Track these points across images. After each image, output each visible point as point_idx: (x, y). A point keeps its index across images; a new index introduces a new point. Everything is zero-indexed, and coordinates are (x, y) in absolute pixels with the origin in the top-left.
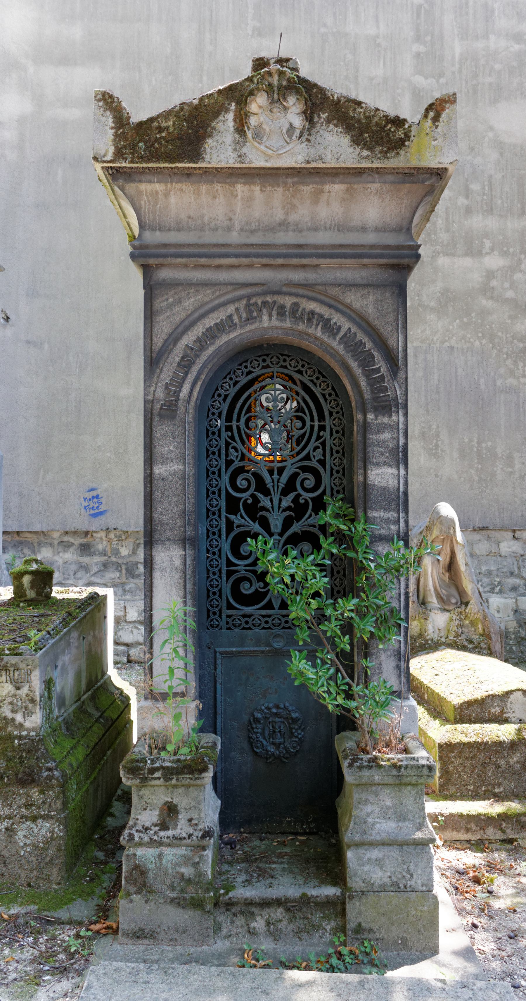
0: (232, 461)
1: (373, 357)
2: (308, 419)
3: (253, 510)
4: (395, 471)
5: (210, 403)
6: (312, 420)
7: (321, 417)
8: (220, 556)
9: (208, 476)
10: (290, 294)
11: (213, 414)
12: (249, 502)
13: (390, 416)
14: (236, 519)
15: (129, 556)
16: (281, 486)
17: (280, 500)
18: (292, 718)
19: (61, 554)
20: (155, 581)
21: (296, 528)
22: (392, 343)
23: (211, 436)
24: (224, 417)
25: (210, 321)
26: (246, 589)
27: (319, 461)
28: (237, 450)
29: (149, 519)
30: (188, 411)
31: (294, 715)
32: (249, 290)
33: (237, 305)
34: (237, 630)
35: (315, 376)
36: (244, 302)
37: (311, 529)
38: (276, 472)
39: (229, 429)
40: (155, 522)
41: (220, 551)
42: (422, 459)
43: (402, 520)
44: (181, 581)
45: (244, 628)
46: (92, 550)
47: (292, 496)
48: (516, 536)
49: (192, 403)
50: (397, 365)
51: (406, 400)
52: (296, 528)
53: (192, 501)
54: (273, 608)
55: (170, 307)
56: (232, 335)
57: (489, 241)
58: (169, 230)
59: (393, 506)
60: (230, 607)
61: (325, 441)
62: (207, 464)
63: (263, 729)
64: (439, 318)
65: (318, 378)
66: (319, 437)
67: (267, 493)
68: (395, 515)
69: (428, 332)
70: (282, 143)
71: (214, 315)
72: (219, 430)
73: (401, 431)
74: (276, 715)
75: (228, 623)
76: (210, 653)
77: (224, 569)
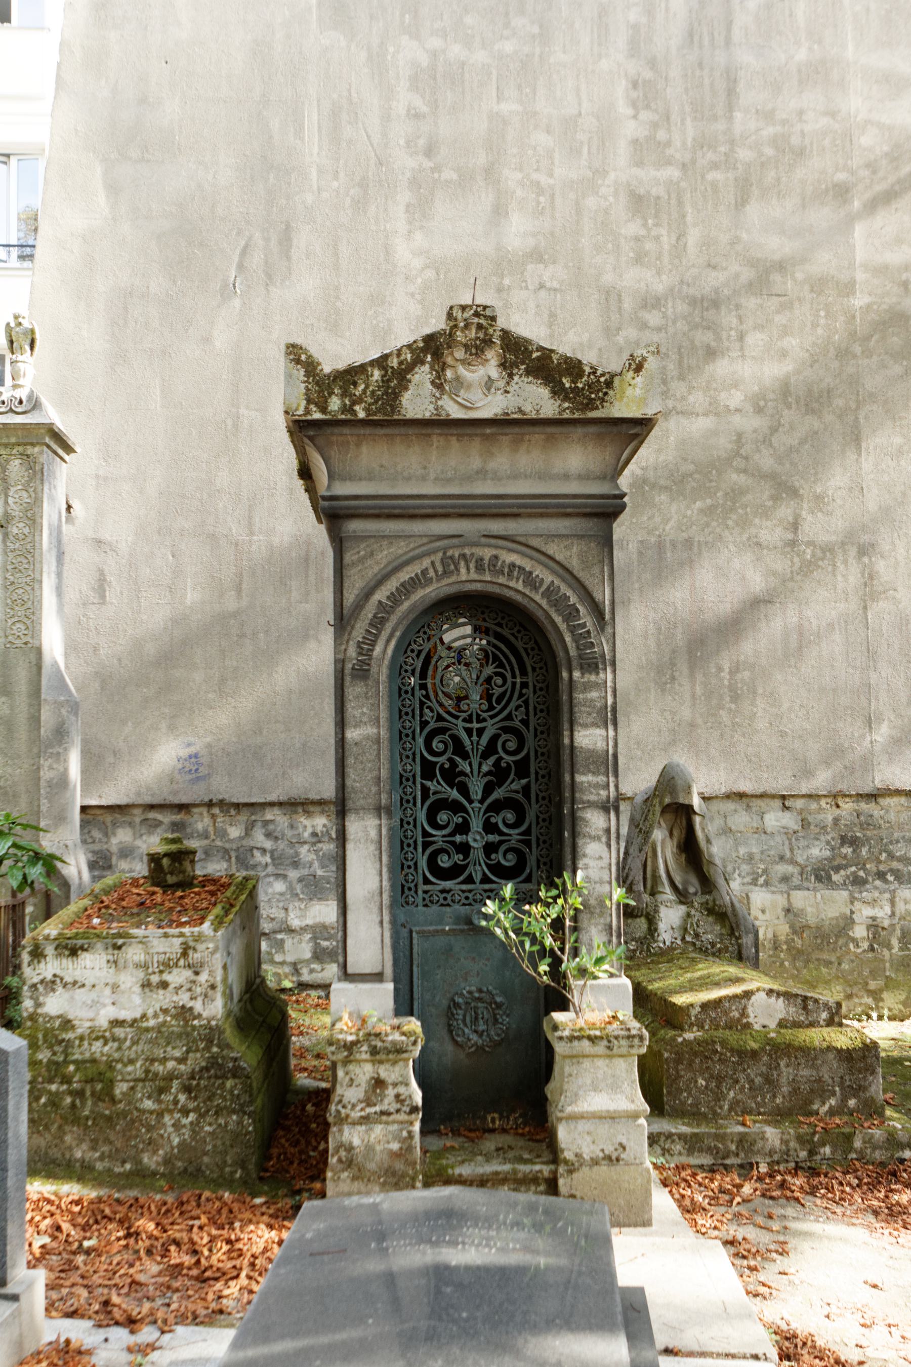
0: (427, 723)
1: (578, 611)
2: (509, 676)
3: (451, 776)
4: (603, 732)
5: (402, 659)
6: (514, 676)
7: (524, 673)
8: (415, 826)
9: (401, 739)
10: (489, 546)
11: (406, 671)
12: (447, 766)
13: (598, 674)
14: (432, 785)
15: (241, 838)
16: (481, 748)
17: (480, 765)
18: (496, 1003)
19: (144, 837)
20: (348, 853)
21: (499, 794)
22: (598, 596)
23: (404, 695)
24: (417, 674)
25: (405, 575)
26: (444, 862)
27: (522, 721)
28: (432, 711)
29: (342, 786)
30: (382, 671)
31: (498, 999)
32: (446, 542)
33: (433, 558)
34: (435, 908)
35: (516, 630)
36: (440, 554)
37: (514, 795)
38: (475, 733)
39: (423, 687)
40: (348, 790)
41: (415, 820)
42: (652, 697)
43: (612, 785)
44: (377, 852)
45: (442, 905)
46: (189, 830)
47: (491, 760)
48: (787, 803)
49: (386, 662)
50: (604, 619)
51: (614, 656)
52: (499, 794)
53: (387, 766)
54: (473, 882)
55: (362, 560)
56: (428, 590)
57: (739, 393)
58: (360, 479)
59: (603, 770)
60: (426, 881)
61: (527, 699)
62: (400, 725)
63: (464, 1016)
64: (673, 499)
65: (519, 632)
66: (521, 695)
67: (465, 756)
68: (605, 779)
69: (657, 519)
70: (483, 396)
71: (409, 568)
72: (413, 689)
73: (609, 690)
74: (480, 999)
75: (424, 899)
76: (404, 932)
77: (420, 840)
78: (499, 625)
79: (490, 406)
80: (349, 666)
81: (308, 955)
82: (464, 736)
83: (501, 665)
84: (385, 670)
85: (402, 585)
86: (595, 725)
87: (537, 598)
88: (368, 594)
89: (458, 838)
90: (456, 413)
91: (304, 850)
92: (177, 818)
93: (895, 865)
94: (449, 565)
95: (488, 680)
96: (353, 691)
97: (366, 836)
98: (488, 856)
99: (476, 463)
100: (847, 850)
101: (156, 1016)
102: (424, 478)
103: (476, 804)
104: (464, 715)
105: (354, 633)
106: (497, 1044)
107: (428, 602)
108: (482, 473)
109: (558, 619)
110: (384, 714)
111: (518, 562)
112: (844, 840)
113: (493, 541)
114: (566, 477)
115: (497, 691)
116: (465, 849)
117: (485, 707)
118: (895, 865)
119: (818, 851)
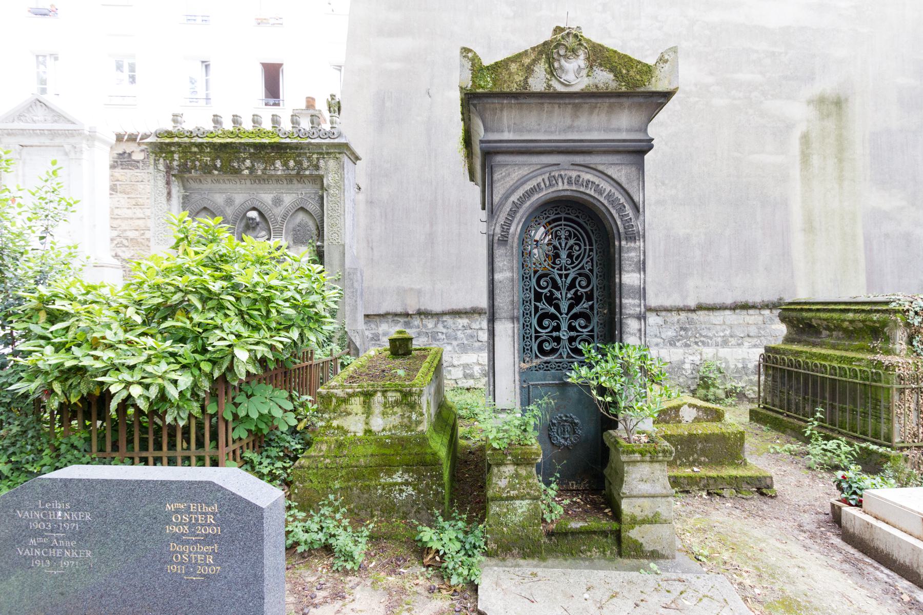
2: (582, 245)
3: (550, 300)
4: (638, 275)
7: (591, 245)
22: (636, 199)
25: (527, 187)
26: (547, 347)
29: (492, 305)
34: (541, 371)
37: (585, 311)
47: (573, 291)
49: (517, 236)
55: (503, 178)
59: (637, 296)
66: (589, 256)
67: (558, 289)
74: (566, 421)
77: (534, 335)
78: (578, 217)
79: (580, 84)
80: (496, 238)
81: (461, 376)
82: (558, 278)
83: (578, 239)
84: (516, 240)
85: (526, 192)
86: (633, 271)
87: (602, 199)
88: (506, 197)
89: (554, 334)
90: (560, 88)
91: (459, 333)
92: (406, 320)
93: (702, 339)
94: (553, 181)
95: (571, 248)
96: (499, 252)
97: (506, 331)
98: (570, 343)
99: (568, 121)
100: (682, 333)
101: (390, 430)
102: (538, 131)
103: (564, 316)
104: (558, 267)
105: (499, 220)
106: (575, 445)
107: (540, 202)
108: (571, 128)
109: (613, 212)
110: (515, 265)
111: (591, 180)
112: (682, 329)
113: (577, 168)
114: (619, 130)
115: (576, 254)
116: (558, 340)
117: (569, 262)
118: (702, 339)
119: (670, 333)
